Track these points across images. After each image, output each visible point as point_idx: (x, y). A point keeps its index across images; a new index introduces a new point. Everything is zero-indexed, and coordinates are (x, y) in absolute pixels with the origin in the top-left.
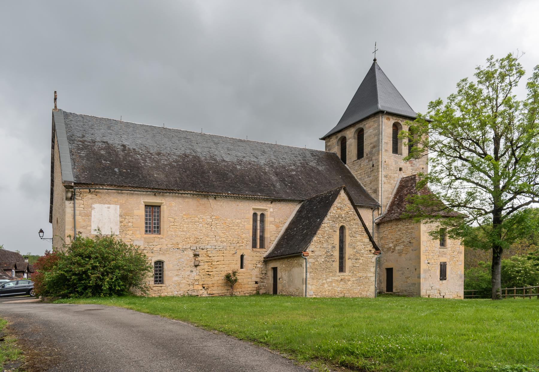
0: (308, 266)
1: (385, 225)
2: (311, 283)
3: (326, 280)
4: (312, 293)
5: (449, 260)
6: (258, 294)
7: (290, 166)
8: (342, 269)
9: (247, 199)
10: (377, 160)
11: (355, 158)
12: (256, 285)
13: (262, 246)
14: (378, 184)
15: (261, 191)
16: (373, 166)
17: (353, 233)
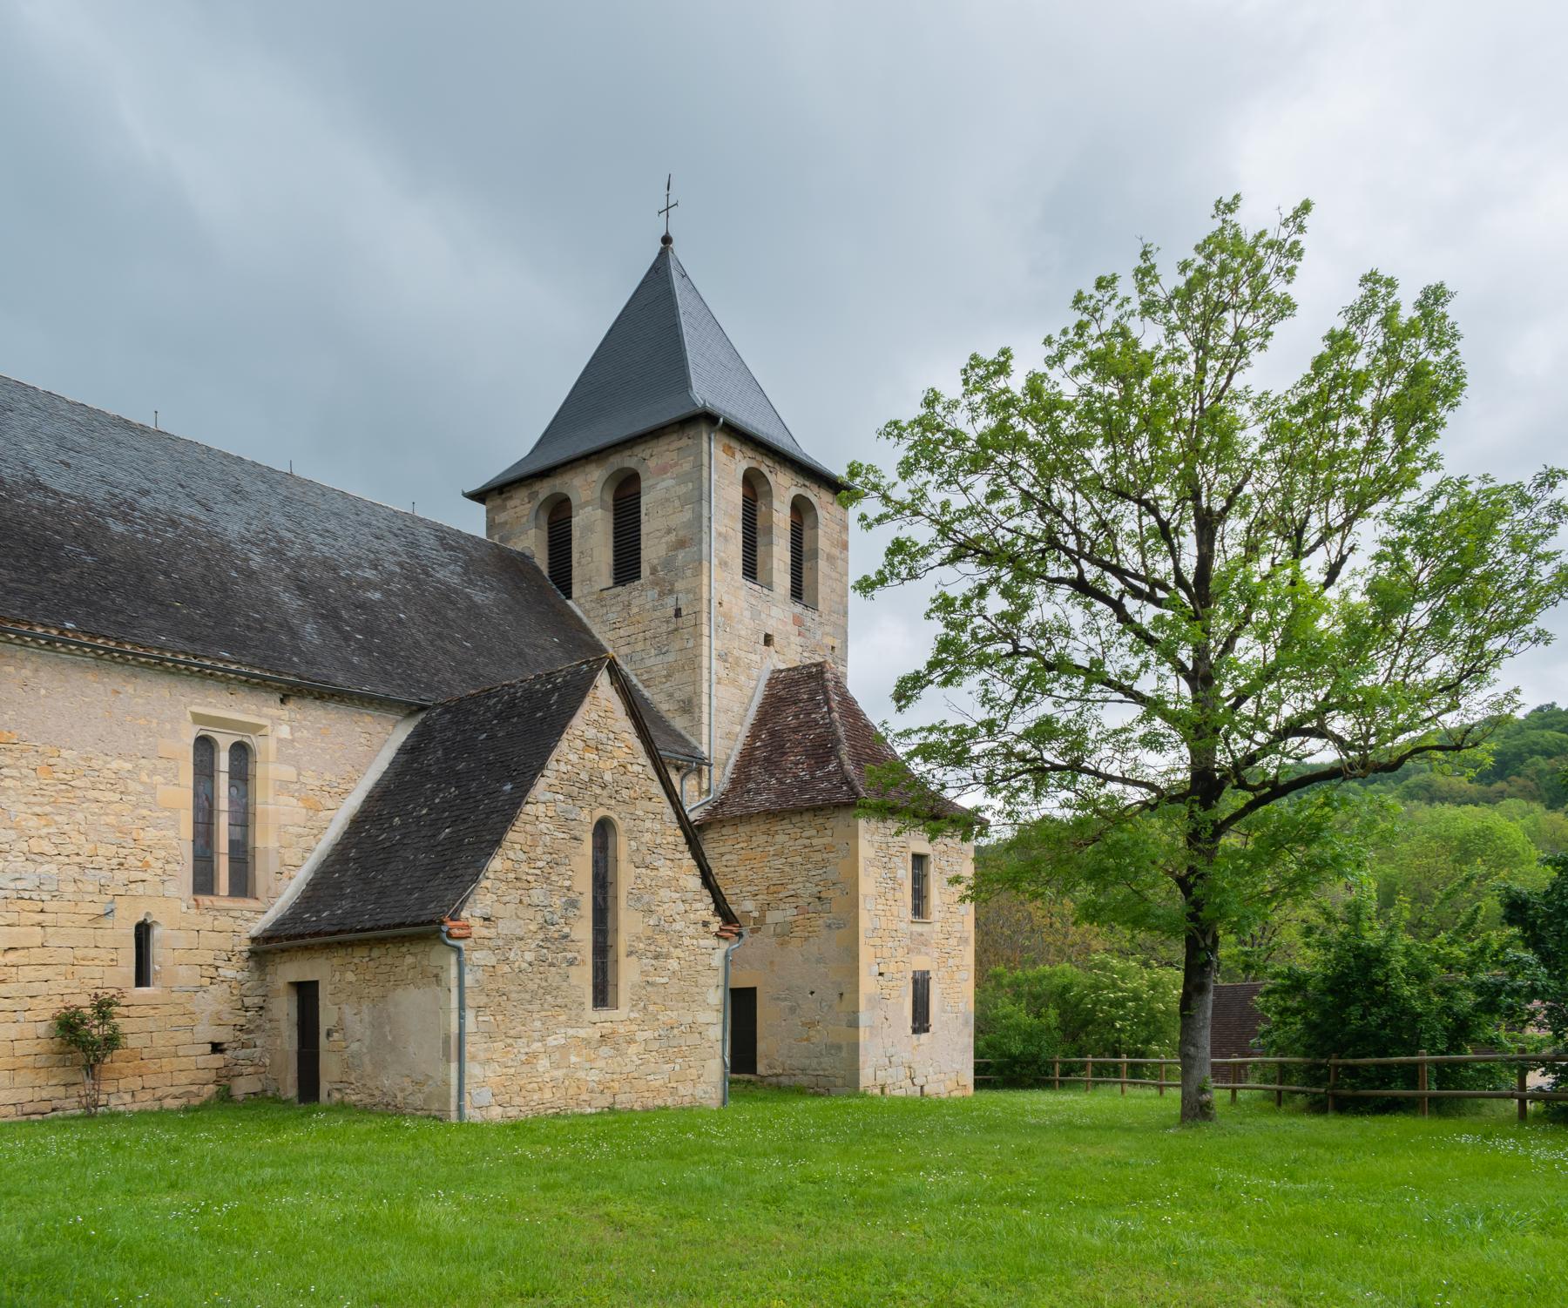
0: (469, 980)
1: (727, 831)
2: (482, 1056)
3: (542, 1039)
4: (485, 1097)
5: (935, 966)
6: (225, 1097)
7: (358, 566)
8: (603, 994)
9: (161, 666)
10: (695, 593)
11: (605, 577)
12: (217, 1060)
13: (242, 885)
14: (696, 683)
15: (236, 644)
16: (678, 613)
17: (643, 849)
